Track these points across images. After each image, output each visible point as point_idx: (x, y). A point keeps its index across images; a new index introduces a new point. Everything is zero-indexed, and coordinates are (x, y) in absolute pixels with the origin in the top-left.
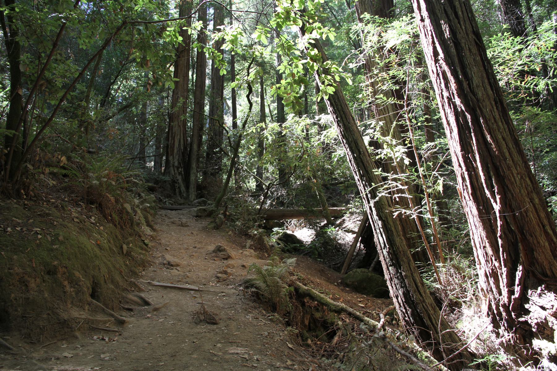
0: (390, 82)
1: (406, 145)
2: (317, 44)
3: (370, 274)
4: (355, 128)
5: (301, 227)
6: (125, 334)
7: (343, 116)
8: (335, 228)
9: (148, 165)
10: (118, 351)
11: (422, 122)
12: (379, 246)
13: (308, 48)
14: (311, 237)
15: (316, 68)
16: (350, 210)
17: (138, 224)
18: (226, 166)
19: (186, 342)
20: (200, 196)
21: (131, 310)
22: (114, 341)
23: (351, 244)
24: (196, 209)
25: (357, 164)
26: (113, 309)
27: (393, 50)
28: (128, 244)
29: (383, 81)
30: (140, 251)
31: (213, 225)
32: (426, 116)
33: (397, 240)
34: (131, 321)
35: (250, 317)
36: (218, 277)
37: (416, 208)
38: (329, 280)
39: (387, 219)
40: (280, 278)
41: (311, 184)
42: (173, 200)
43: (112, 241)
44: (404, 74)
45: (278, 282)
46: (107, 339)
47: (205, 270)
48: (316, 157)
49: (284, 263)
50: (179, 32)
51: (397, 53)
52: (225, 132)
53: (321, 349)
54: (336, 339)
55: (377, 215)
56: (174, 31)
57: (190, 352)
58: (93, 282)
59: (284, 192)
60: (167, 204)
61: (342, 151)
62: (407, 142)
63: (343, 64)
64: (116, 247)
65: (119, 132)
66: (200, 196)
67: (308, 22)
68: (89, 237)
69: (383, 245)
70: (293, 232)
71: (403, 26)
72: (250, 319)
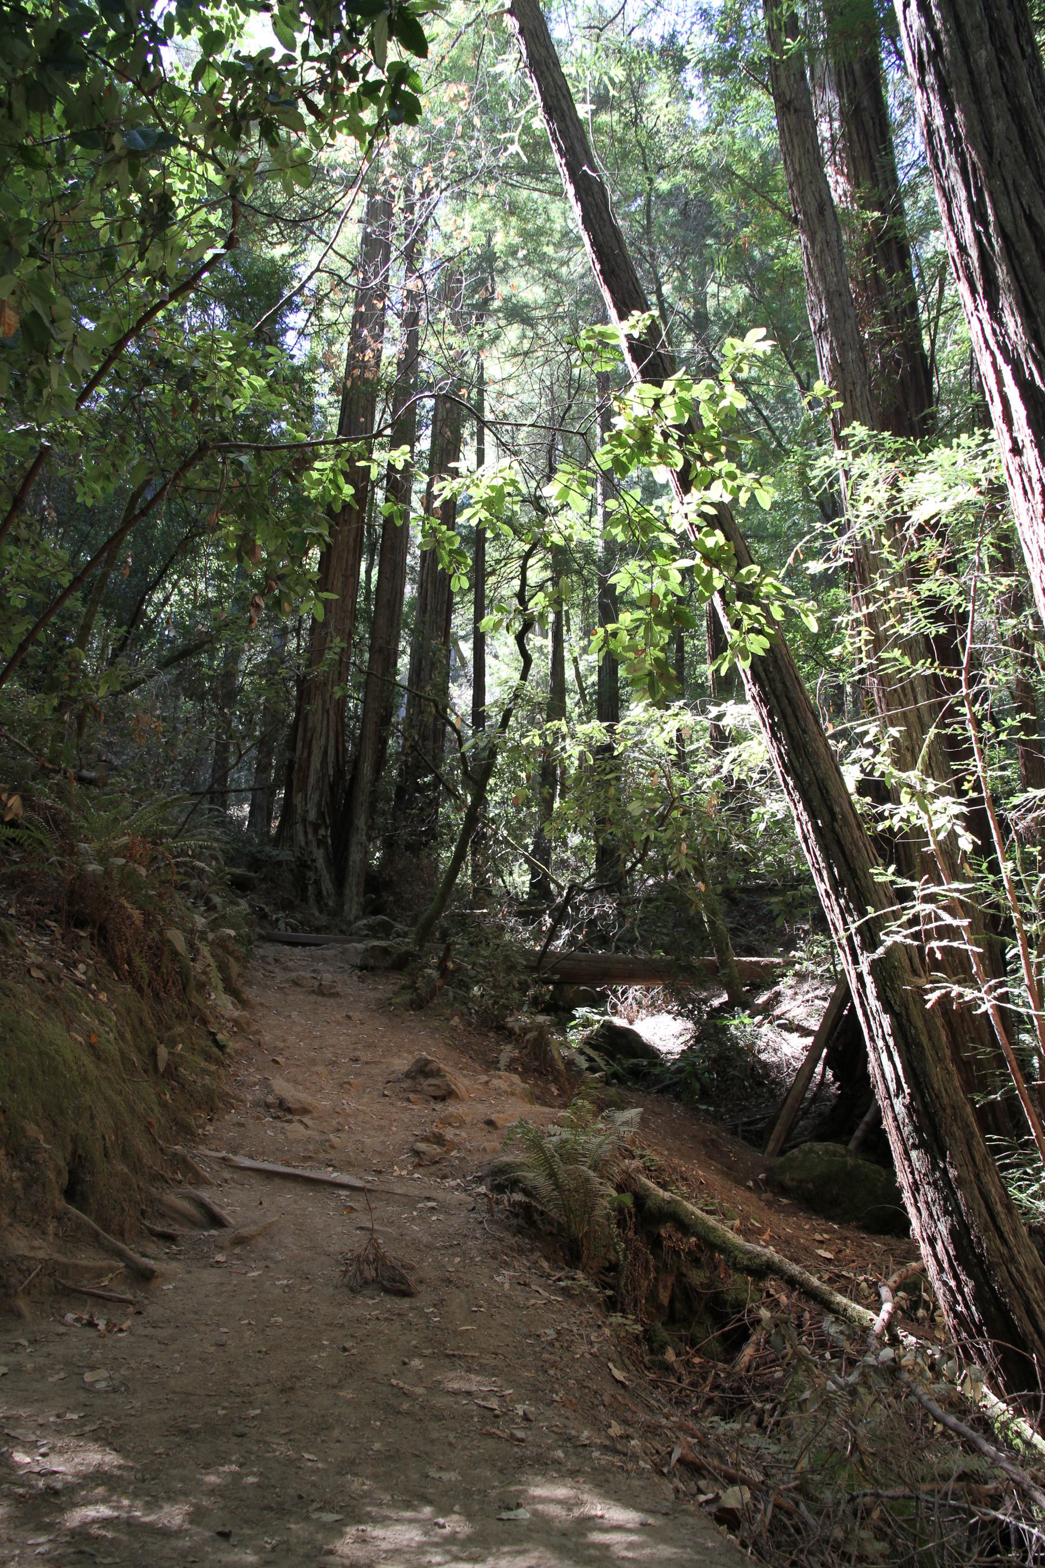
0: (920, 615)
1: (966, 792)
2: (720, 518)
3: (850, 1161)
4: (821, 745)
5: (654, 1008)
6: (154, 1311)
7: (789, 710)
8: (751, 1016)
9: (233, 811)
10: (133, 1365)
11: (1013, 731)
12: (881, 1085)
13: (699, 529)
14: (682, 1039)
15: (718, 583)
16: (797, 967)
17: (201, 987)
18: (449, 826)
19: (323, 1348)
20: (373, 908)
21: (169, 1238)
22: (121, 1330)
23: (798, 1065)
24: (360, 946)
25: (825, 849)
26: (121, 1234)
27: (930, 527)
28: (172, 1043)
29: (901, 610)
30: (203, 1064)
31: (407, 997)
32: (1024, 715)
33: (936, 1073)
34: (170, 1269)
35: (504, 1278)
36: (417, 1153)
37: (993, 982)
38: (733, 1173)
39: (907, 1009)
40: (594, 1167)
41: (689, 893)
42: (298, 916)
43: (128, 1036)
44: (960, 594)
45: (587, 1180)
46: (102, 1326)
47: (381, 1128)
48: (703, 817)
49: (607, 1119)
50: (345, 474)
51: (941, 535)
52: (449, 729)
53: (705, 1379)
54: (748, 1352)
55: (878, 998)
56: (332, 470)
57: (335, 1381)
58: (74, 1152)
59: (609, 907)
60: (282, 925)
61: (778, 805)
62: (966, 786)
63: (790, 560)
64: (140, 1051)
65: (162, 726)
66: (373, 908)
67: (700, 458)
68: (69, 1023)
69: (893, 1087)
70: (631, 1022)
71: (960, 462)
72: (507, 1286)
